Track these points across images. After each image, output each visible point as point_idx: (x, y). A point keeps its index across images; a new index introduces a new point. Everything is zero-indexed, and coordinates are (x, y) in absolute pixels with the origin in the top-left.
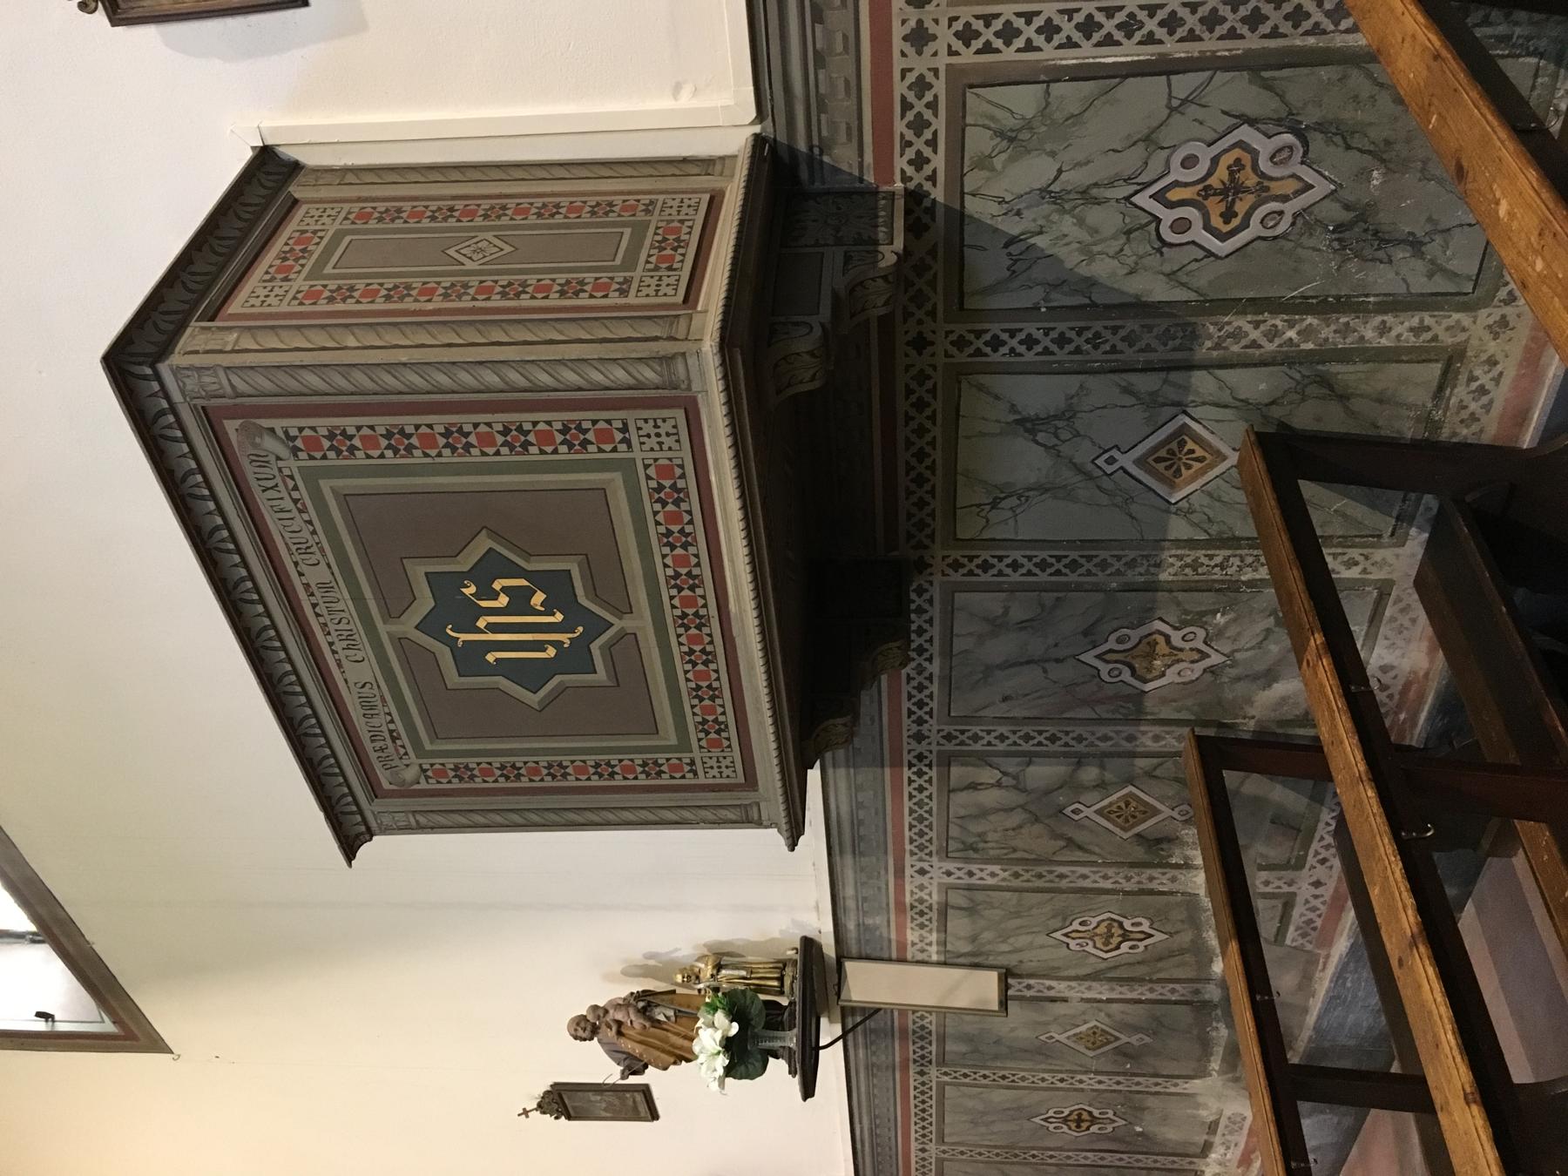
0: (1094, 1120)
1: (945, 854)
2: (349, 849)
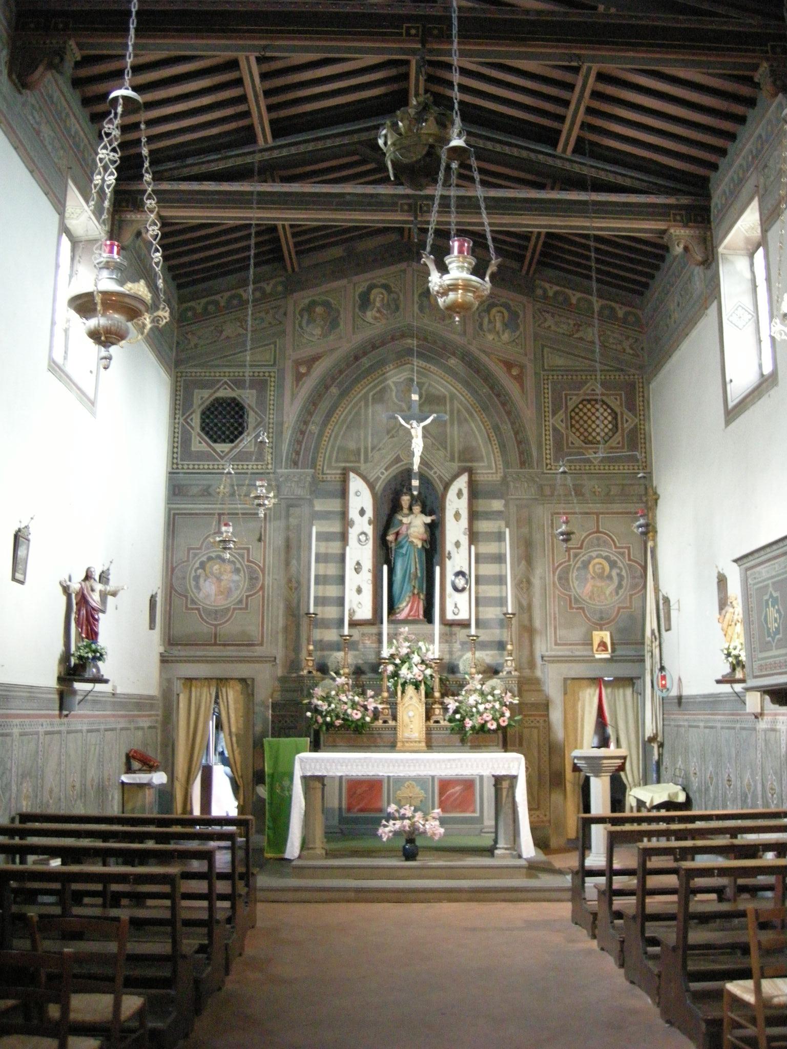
0: (730, 786)
2: (735, 561)
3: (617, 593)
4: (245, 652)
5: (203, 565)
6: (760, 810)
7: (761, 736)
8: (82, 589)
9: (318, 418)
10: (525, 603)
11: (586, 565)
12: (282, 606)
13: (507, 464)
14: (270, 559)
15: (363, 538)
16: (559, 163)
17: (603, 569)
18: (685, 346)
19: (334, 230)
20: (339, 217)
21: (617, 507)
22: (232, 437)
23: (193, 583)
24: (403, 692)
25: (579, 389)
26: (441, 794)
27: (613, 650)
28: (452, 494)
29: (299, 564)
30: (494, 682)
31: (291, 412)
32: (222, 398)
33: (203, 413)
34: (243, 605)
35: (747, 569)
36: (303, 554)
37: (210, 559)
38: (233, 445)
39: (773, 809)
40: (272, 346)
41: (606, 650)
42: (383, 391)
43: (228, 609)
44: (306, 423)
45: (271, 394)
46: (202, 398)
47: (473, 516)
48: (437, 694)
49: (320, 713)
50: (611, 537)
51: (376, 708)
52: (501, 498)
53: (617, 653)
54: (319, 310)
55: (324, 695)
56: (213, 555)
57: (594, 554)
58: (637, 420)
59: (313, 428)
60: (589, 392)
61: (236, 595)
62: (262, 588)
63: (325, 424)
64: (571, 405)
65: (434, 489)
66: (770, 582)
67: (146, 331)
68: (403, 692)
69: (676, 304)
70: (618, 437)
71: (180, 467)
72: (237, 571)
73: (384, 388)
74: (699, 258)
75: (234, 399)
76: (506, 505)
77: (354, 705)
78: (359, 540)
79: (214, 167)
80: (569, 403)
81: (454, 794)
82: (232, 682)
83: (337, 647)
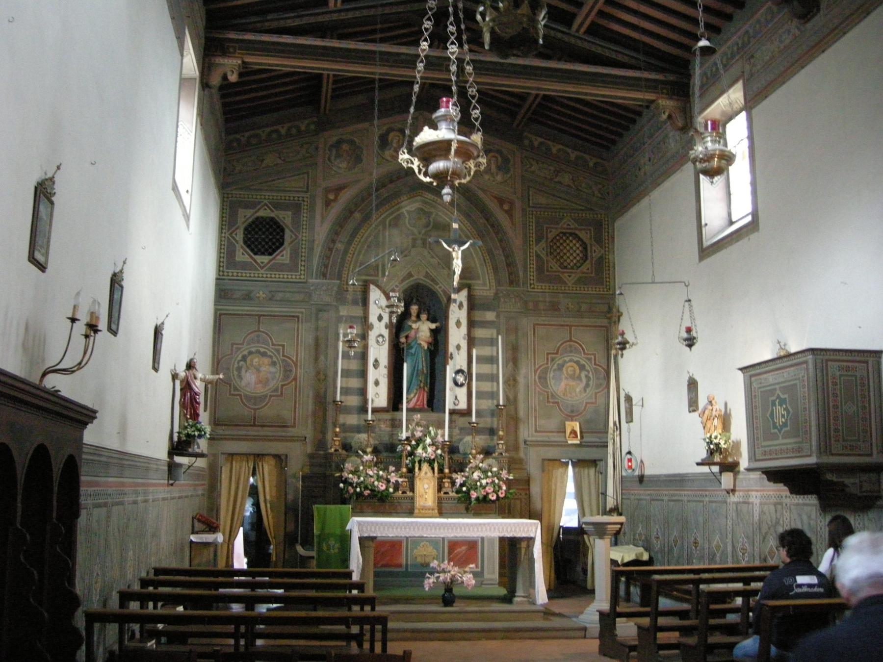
0: (696, 547)
1: (761, 504)
2: (741, 369)
3: (585, 391)
4: (280, 432)
5: (244, 358)
6: (730, 565)
7: (732, 508)
8: (187, 376)
9: (344, 237)
10: (511, 397)
11: (561, 367)
12: (311, 395)
13: (499, 283)
14: (302, 354)
15: (380, 339)
16: (573, 41)
17: (574, 371)
18: (656, 194)
19: (273, 74)
20: (351, 69)
21: (586, 321)
22: (270, 250)
23: (236, 373)
24: (420, 469)
25: (558, 223)
26: (450, 553)
27: (582, 437)
28: (453, 307)
29: (326, 358)
30: (490, 461)
31: (321, 231)
32: (262, 217)
33: (246, 229)
34: (279, 393)
35: (751, 376)
36: (330, 352)
37: (250, 353)
38: (271, 257)
39: (743, 564)
40: (306, 176)
41: (577, 437)
42: (398, 218)
43: (266, 396)
44: (334, 242)
45: (304, 214)
46: (245, 216)
47: (471, 324)
48: (447, 471)
49: (351, 484)
50: (581, 346)
51: (397, 481)
52: (494, 310)
53: (585, 440)
54: (345, 147)
55: (353, 469)
56: (253, 350)
57: (567, 359)
58: (603, 251)
59: (340, 246)
60: (565, 226)
61: (272, 384)
62: (295, 379)
63: (350, 243)
64: (551, 236)
65: (440, 302)
66: (777, 386)
67: (472, 173)
68: (420, 469)
69: (647, 158)
70: (587, 265)
71: (226, 274)
72: (274, 364)
73: (399, 215)
74: (680, 124)
75: (272, 219)
76: (498, 316)
77: (379, 478)
78: (378, 342)
79: (290, 23)
80: (549, 235)
81: (463, 551)
82: (267, 457)
83: (358, 429)
